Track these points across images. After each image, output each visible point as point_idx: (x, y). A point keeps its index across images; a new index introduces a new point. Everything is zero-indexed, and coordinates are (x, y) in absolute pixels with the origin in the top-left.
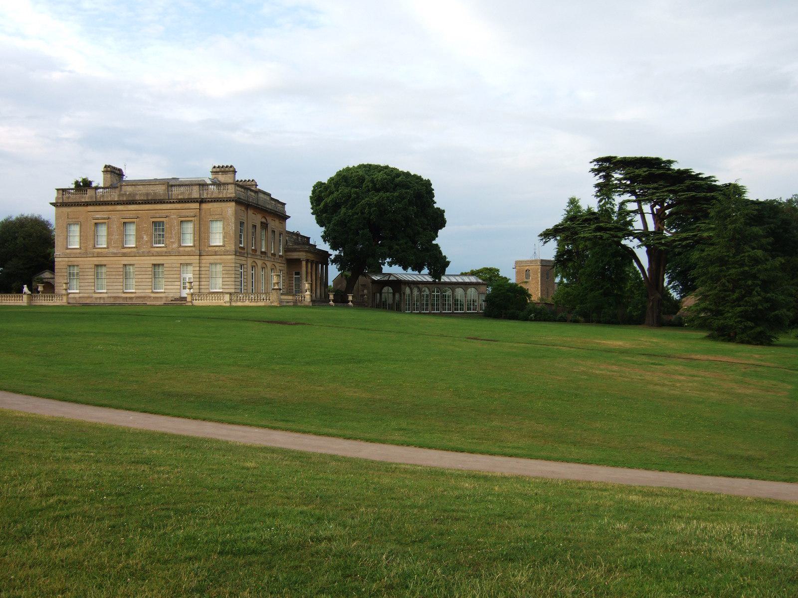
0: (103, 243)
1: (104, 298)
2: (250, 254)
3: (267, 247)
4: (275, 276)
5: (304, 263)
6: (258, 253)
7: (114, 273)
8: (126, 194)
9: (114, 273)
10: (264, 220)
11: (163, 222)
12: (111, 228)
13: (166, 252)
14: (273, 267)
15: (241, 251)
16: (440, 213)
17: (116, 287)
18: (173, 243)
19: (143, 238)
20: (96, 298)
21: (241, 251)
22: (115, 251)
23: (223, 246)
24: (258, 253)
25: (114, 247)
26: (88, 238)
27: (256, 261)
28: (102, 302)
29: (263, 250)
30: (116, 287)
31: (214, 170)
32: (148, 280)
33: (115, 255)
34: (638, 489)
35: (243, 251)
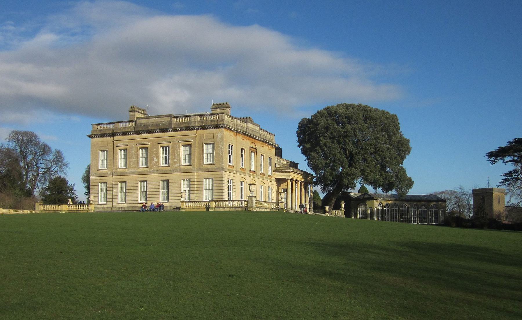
0: (121, 164)
1: (124, 208)
2: (239, 171)
3: (256, 167)
4: (120, 152)
5: (289, 181)
6: (247, 171)
7: (132, 188)
8: (141, 126)
9: (132, 188)
10: (253, 146)
11: (169, 147)
12: (130, 152)
13: (170, 170)
14: (262, 184)
15: (229, 168)
16: (410, 179)
17: (133, 199)
18: (176, 163)
20: (119, 208)
21: (229, 168)
22: (133, 170)
23: (213, 164)
24: (247, 171)
25: (133, 168)
26: (111, 161)
27: (245, 177)
28: (123, 210)
29: (253, 169)
30: (133, 199)
31: (214, 107)
32: (129, 188)
33: (133, 174)
34: (450, 206)
35: (232, 169)
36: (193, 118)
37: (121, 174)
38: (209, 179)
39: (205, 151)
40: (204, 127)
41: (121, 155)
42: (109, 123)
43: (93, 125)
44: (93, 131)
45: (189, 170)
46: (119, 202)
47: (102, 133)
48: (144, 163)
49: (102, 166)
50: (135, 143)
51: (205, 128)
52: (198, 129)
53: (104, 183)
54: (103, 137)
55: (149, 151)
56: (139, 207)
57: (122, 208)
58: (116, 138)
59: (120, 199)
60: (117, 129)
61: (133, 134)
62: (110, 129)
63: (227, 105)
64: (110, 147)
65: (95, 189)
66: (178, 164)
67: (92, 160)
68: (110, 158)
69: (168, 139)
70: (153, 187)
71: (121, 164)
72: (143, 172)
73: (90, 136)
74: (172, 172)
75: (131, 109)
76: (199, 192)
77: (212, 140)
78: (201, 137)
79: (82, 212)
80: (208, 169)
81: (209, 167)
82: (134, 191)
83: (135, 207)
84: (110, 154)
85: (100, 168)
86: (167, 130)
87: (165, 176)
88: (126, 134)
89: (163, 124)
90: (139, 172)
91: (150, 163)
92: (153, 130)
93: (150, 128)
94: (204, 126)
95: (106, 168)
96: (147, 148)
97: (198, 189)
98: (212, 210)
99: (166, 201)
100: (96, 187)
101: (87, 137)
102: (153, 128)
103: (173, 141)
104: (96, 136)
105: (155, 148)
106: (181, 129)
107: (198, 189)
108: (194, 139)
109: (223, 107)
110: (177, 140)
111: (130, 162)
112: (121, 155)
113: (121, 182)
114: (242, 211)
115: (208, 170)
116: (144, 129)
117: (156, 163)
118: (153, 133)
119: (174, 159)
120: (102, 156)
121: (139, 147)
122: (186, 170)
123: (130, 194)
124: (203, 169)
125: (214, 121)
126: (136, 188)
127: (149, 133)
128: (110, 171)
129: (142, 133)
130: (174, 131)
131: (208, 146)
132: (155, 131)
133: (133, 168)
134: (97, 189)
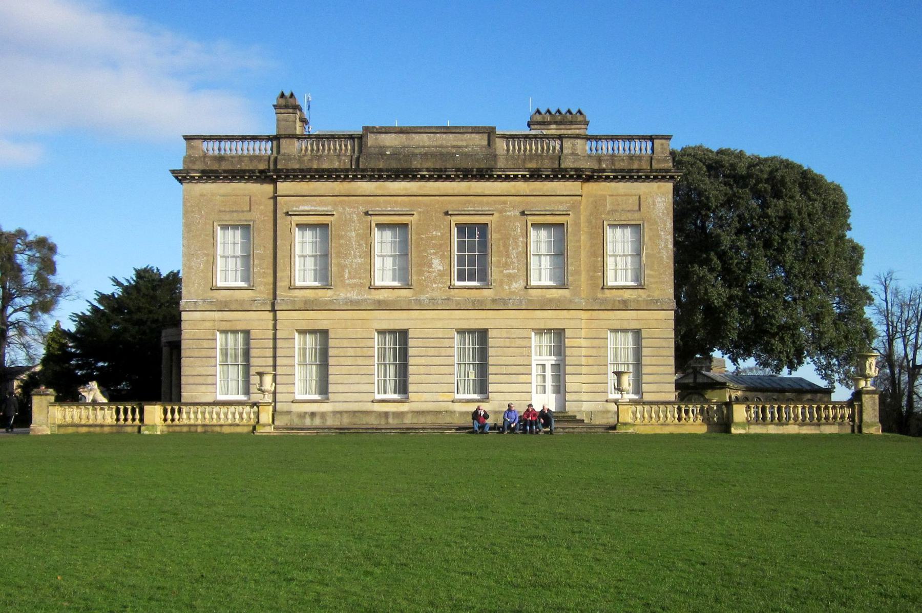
0: (303, 272)
1: (323, 415)
4: (297, 233)
7: (351, 352)
8: (383, 154)
11: (484, 227)
19: (431, 265)
20: (302, 415)
22: (353, 295)
31: (538, 118)
33: (355, 306)
36: (567, 144)
37: (308, 306)
38: (235, 332)
39: (298, 250)
40: (611, 175)
41: (303, 244)
42: (254, 138)
43: (188, 138)
44: (188, 159)
45: (558, 300)
46: (298, 397)
47: (225, 166)
48: (310, 275)
49: (228, 274)
50: (362, 209)
51: (615, 178)
52: (589, 179)
53: (235, 332)
54: (231, 181)
55: (413, 236)
56: (463, 414)
57: (313, 414)
58: (284, 187)
59: (299, 387)
60: (289, 158)
61: (355, 178)
62: (259, 158)
63: (580, 118)
64: (261, 215)
65: (204, 353)
66: (522, 283)
67: (189, 256)
68: (263, 250)
69: (481, 203)
70: (432, 352)
71: (303, 272)
72: (395, 301)
73: (182, 177)
74: (499, 305)
75: (282, 102)
76: (595, 370)
77: (637, 215)
78: (597, 203)
79: (226, 430)
80: (625, 302)
81: (627, 295)
82: (360, 361)
83: (367, 413)
84: (263, 238)
85: (220, 284)
86: (483, 174)
87: (552, 319)
88: (329, 178)
89: (466, 155)
90: (379, 302)
91: (420, 273)
92: (435, 170)
93: (416, 164)
94: (428, 170)
95: (243, 285)
96: (406, 225)
97: (591, 361)
98: (742, 431)
99: (317, 397)
100: (205, 344)
101: (171, 176)
102: (430, 165)
103: (500, 212)
104: (209, 175)
105: (437, 228)
106: (535, 175)
107: (591, 361)
108: (575, 207)
109: (571, 123)
110: (514, 207)
111: (342, 268)
112: (303, 244)
113: (302, 332)
114: (112, 433)
115: (625, 306)
116: (394, 165)
117: (441, 274)
118: (430, 178)
119: (506, 265)
120: (228, 243)
121: (375, 220)
122: (551, 300)
123: (344, 370)
124: (605, 300)
125: (640, 158)
126: (367, 352)
127: (414, 178)
128: (262, 292)
129: (389, 178)
130: (507, 178)
131: (230, 232)
132: (440, 175)
133: (353, 286)
134: (210, 353)
